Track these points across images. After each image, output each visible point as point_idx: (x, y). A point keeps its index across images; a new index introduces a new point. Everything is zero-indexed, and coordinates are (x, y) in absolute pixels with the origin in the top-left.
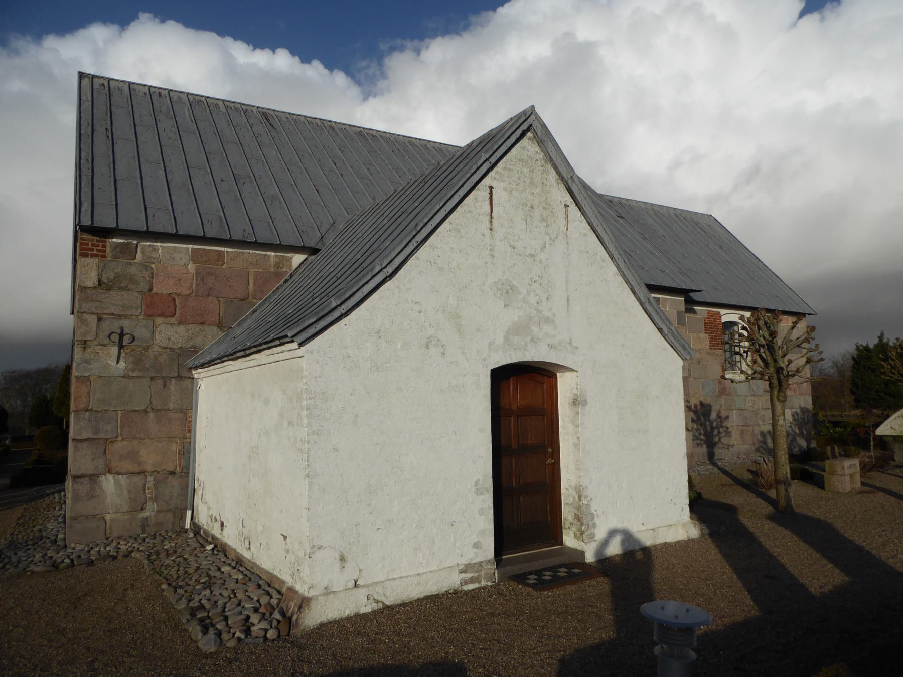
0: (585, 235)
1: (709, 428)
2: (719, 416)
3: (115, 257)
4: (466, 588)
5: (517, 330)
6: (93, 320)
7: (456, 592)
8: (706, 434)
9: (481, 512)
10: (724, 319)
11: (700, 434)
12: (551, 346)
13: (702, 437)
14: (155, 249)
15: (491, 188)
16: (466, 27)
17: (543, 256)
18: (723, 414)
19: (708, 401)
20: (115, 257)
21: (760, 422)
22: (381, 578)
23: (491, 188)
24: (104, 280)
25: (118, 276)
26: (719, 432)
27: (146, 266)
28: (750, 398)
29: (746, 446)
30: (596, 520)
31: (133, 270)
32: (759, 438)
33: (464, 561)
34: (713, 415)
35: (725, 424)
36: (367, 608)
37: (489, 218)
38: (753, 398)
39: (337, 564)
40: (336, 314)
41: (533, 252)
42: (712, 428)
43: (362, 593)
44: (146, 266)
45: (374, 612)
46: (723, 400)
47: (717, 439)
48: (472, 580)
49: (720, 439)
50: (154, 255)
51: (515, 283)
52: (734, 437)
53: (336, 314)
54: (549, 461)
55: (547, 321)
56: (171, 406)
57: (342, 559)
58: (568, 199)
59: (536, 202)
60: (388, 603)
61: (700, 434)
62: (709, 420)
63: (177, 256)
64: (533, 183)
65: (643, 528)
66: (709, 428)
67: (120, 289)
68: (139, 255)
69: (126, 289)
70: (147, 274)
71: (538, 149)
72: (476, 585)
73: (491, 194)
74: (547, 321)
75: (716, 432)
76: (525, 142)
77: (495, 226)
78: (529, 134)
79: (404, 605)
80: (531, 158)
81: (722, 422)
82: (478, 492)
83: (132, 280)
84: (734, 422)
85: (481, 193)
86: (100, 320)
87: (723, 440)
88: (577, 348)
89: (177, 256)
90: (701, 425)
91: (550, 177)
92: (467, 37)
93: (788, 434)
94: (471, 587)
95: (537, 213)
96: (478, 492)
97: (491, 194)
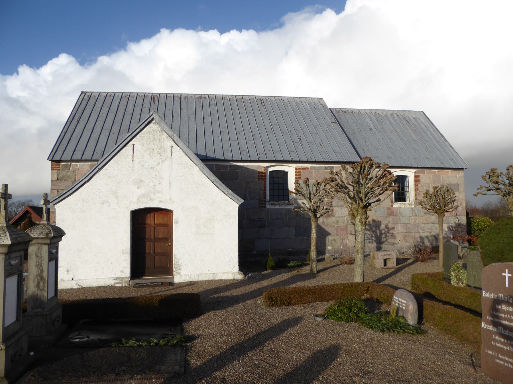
0: (181, 157)
1: (378, 234)
2: (387, 227)
3: (63, 170)
4: (116, 285)
5: (143, 196)
6: (56, 192)
7: (112, 286)
8: (376, 237)
9: (124, 260)
10: (396, 174)
11: (372, 237)
12: (160, 201)
13: (374, 238)
14: (76, 165)
15: (134, 145)
16: (281, 25)
17: (158, 168)
18: (390, 226)
19: (380, 219)
20: (63, 170)
21: (420, 231)
22: (82, 278)
23: (134, 145)
24: (59, 178)
25: (64, 176)
26: (386, 236)
27: (74, 171)
28: (413, 217)
29: (408, 244)
30: (181, 267)
31: (69, 173)
32: (419, 240)
33: (116, 276)
34: (383, 227)
35: (391, 231)
36: (75, 287)
37: (132, 156)
38: (415, 217)
39: (66, 273)
40: (66, 195)
41: (153, 167)
42: (381, 234)
43: (73, 283)
44: (74, 171)
45: (78, 289)
46: (391, 219)
47: (384, 240)
48: (119, 283)
49: (386, 240)
50: (77, 167)
51: (143, 179)
52: (398, 239)
53: (66, 195)
54: (170, 244)
55: (158, 192)
56: (321, 220)
57: (68, 271)
58: (173, 143)
59: (156, 147)
60: (84, 286)
61: (372, 237)
62: (379, 229)
63: (84, 167)
64: (154, 140)
65: (209, 272)
66: (378, 234)
67: (65, 180)
68: (71, 168)
69: (66, 180)
70: (74, 175)
71: (158, 126)
72: (121, 285)
73: (133, 147)
74: (158, 192)
75: (383, 236)
76: (151, 125)
77: (134, 159)
78: (154, 121)
79: (89, 288)
80: (154, 131)
81: (389, 231)
82: (123, 253)
83: (68, 177)
84: (399, 230)
85: (129, 147)
86: (58, 191)
87: (389, 240)
88: (174, 202)
89: (84, 167)
90: (373, 232)
91: (164, 136)
92: (270, 37)
93: (444, 238)
94: (118, 285)
95: (156, 151)
96: (123, 253)
97: (133, 147)
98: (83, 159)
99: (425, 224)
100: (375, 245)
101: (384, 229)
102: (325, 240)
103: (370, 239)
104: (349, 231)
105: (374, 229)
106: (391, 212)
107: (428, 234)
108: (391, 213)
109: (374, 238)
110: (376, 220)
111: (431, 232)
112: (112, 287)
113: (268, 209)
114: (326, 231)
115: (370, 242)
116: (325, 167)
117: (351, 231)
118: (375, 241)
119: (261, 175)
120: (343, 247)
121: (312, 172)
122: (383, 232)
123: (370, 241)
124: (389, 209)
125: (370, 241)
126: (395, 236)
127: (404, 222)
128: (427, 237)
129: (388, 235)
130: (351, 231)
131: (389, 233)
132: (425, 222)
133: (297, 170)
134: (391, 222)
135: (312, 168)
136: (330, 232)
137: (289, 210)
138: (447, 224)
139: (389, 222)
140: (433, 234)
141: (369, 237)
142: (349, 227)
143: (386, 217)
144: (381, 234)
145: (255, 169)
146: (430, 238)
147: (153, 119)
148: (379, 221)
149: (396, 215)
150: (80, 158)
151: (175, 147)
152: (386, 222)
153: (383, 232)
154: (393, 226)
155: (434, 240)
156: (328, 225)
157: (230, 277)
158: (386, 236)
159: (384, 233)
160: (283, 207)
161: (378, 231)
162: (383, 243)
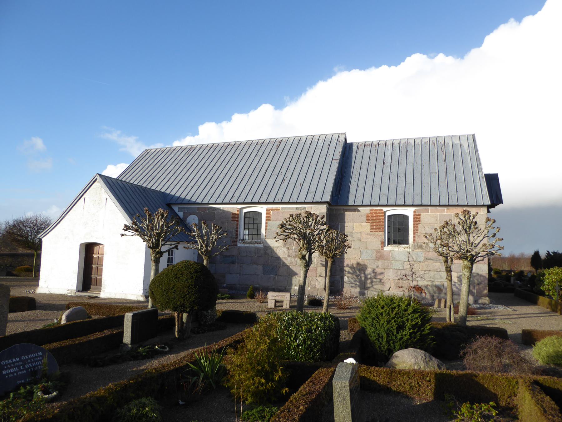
1: (363, 278)
2: (373, 271)
8: (361, 281)
13: (358, 283)
18: (378, 270)
34: (369, 271)
36: (47, 293)
46: (380, 262)
47: (369, 285)
49: (372, 286)
52: (388, 286)
62: (364, 273)
75: (369, 281)
81: (375, 275)
90: (357, 276)
98: (314, 201)
99: (425, 271)
100: (358, 290)
101: (370, 274)
102: (291, 280)
103: (352, 283)
104: (319, 273)
105: (358, 273)
106: (381, 256)
107: (430, 283)
108: (380, 256)
109: (358, 283)
110: (362, 263)
111: (433, 282)
112: (66, 296)
113: (239, 247)
114: (293, 271)
115: (352, 287)
116: (297, 208)
117: (321, 273)
118: (359, 286)
119: (235, 217)
120: (311, 288)
121: (282, 213)
122: (369, 276)
123: (353, 285)
124: (378, 251)
125: (353, 285)
126: (384, 282)
127: (396, 267)
128: (426, 287)
129: (375, 280)
130: (321, 273)
131: (376, 278)
132: (425, 268)
133: (268, 211)
134: (380, 267)
135: (282, 208)
136: (297, 272)
137: (258, 249)
138: (458, 273)
139: (377, 267)
140: (437, 283)
141: (352, 281)
142: (319, 268)
143: (374, 260)
144: (366, 278)
145: (230, 210)
146: (430, 288)
147: (96, 179)
148: (365, 265)
149: (385, 260)
150: (280, 201)
151: (109, 199)
152: (374, 267)
153: (369, 276)
154: (383, 271)
155: (437, 292)
156: (296, 265)
157: (133, 298)
158: (372, 282)
159: (370, 278)
160: (252, 246)
161: (363, 275)
162: (368, 288)
